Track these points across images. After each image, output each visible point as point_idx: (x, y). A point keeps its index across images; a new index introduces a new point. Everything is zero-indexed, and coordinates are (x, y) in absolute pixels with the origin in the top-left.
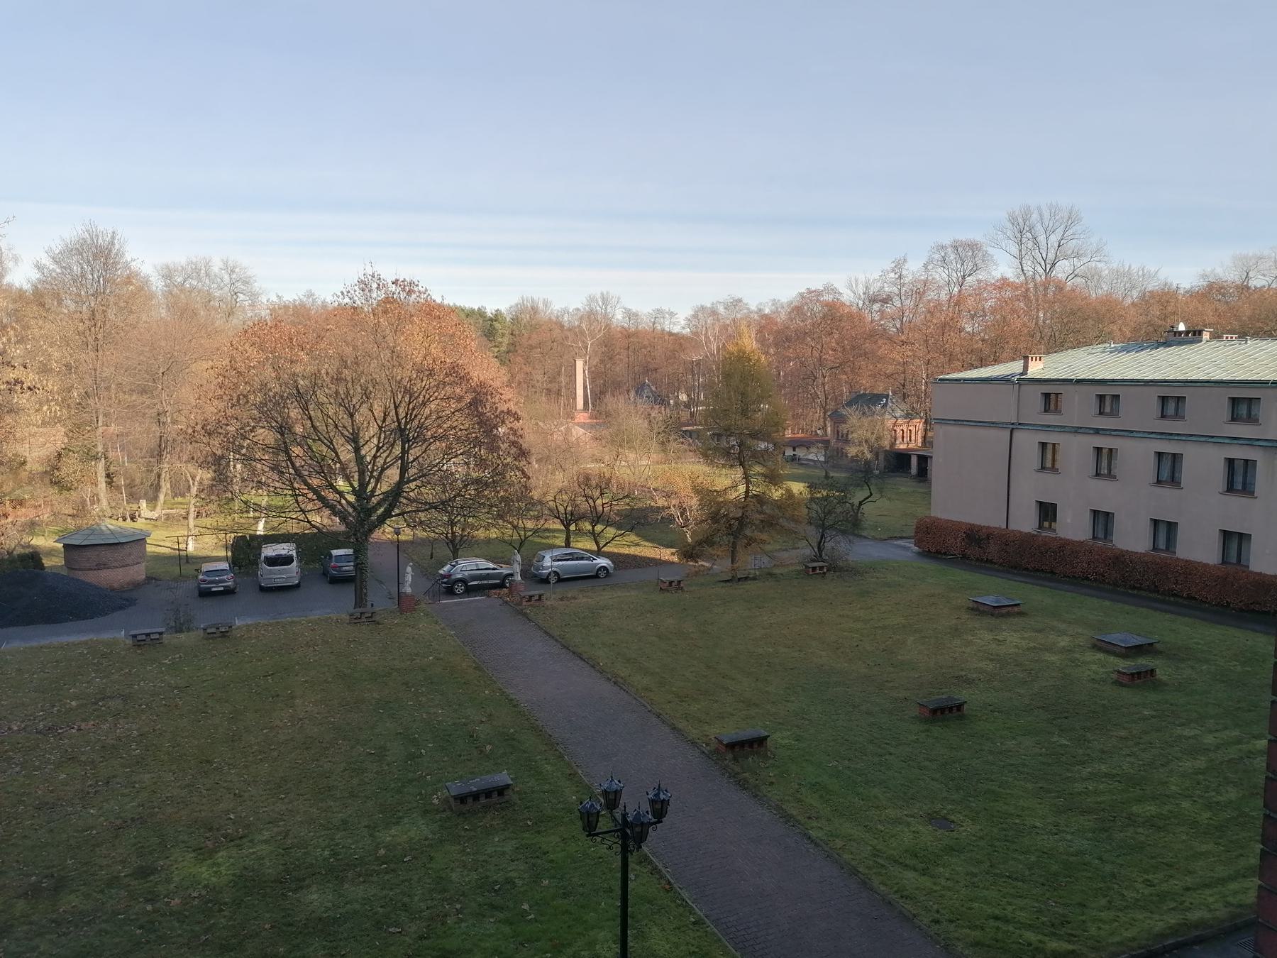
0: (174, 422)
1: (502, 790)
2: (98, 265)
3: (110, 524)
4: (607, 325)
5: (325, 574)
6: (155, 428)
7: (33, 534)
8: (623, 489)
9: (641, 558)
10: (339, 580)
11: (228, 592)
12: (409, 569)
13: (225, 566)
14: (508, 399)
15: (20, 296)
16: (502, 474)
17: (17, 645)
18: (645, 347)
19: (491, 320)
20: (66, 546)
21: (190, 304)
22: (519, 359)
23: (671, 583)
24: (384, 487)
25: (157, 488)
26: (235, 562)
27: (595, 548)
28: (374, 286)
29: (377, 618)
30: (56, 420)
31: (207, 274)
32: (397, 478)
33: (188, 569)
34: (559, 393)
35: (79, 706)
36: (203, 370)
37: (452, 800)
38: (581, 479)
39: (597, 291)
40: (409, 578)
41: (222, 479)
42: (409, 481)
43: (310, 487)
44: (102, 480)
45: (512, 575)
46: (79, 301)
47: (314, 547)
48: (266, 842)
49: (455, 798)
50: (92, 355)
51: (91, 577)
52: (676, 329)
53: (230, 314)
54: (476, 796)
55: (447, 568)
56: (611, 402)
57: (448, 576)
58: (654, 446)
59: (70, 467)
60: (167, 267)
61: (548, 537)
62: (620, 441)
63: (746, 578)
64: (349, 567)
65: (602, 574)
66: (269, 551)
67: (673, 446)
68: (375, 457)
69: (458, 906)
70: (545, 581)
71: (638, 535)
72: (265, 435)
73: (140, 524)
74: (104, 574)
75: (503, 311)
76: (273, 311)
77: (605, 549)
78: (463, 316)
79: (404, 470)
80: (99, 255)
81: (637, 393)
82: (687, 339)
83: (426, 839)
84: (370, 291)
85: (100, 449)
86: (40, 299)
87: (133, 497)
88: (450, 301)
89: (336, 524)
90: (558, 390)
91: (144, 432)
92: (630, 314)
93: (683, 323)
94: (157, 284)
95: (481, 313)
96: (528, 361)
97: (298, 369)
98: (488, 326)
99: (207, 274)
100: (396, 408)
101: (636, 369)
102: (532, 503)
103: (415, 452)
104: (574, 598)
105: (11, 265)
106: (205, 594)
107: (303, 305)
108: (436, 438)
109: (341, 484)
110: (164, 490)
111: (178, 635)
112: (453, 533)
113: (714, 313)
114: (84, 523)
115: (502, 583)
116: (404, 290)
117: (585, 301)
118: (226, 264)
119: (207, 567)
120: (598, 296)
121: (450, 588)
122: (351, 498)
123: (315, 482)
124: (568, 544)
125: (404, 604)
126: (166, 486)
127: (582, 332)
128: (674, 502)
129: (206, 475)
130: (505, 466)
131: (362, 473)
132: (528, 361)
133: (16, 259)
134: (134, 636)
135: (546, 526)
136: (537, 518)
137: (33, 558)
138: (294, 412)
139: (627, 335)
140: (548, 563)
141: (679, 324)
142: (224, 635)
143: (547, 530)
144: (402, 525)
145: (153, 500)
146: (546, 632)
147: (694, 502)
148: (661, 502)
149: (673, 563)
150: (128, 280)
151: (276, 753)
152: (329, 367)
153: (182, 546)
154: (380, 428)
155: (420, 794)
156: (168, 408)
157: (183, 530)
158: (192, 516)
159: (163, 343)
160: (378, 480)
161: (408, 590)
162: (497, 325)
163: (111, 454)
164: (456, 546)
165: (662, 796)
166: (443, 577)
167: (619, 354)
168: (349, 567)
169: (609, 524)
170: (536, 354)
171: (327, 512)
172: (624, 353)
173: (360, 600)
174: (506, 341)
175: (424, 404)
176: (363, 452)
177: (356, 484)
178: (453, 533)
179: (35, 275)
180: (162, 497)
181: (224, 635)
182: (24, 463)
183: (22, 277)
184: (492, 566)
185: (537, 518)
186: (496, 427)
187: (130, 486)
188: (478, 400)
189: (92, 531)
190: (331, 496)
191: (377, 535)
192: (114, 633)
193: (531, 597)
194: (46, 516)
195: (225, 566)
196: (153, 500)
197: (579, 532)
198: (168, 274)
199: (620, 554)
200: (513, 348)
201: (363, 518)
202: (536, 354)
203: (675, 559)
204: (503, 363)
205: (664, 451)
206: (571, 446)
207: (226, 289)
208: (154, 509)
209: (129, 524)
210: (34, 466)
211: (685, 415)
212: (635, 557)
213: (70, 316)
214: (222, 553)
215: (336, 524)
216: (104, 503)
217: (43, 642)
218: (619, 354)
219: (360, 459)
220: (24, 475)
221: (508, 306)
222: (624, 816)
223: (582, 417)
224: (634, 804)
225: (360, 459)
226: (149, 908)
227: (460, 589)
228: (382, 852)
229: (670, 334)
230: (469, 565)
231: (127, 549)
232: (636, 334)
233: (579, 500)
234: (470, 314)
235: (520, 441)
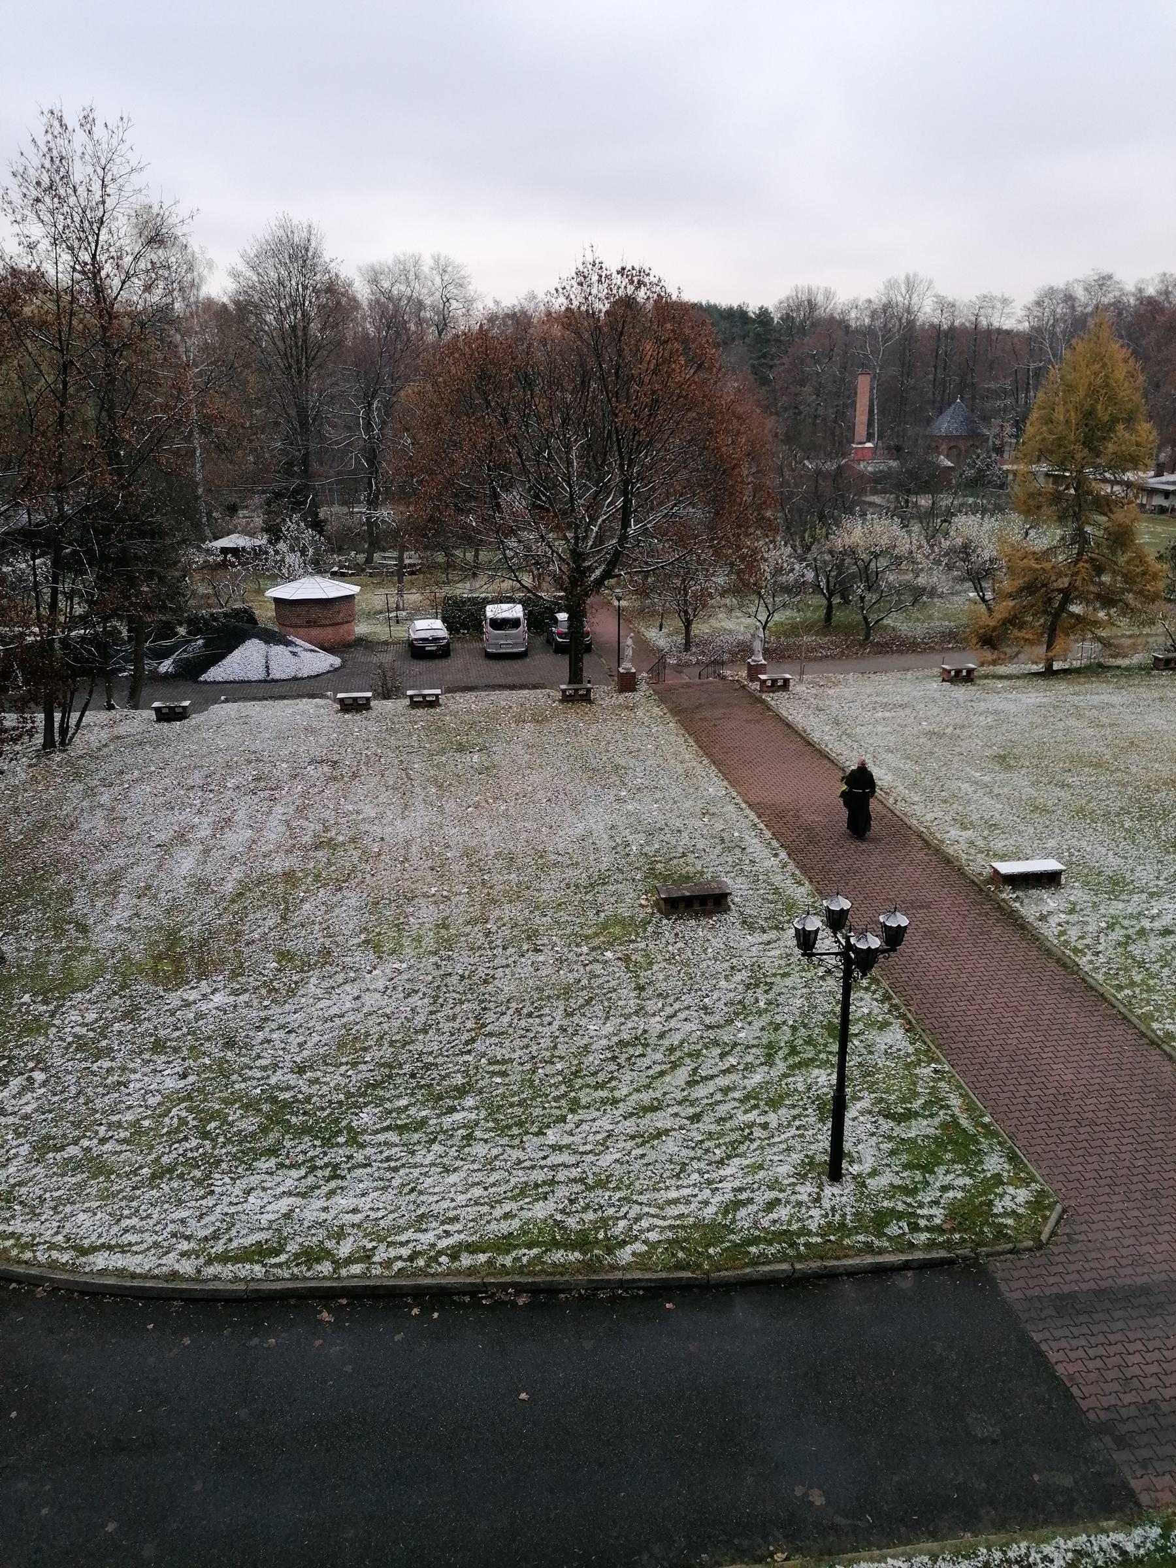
2: (295, 268)
12: (629, 642)
28: (595, 278)
31: (417, 277)
37: (662, 903)
52: (1008, 324)
60: (373, 269)
63: (267, 667)
75: (771, 309)
76: (492, 319)
80: (298, 254)
93: (1020, 313)
94: (362, 291)
99: (417, 277)
105: (205, 272)
107: (524, 313)
111: (385, 702)
113: (1069, 298)
117: (882, 288)
118: (437, 262)
120: (902, 280)
133: (210, 265)
141: (1013, 318)
183: (218, 287)
207: (438, 294)
231: (336, 608)
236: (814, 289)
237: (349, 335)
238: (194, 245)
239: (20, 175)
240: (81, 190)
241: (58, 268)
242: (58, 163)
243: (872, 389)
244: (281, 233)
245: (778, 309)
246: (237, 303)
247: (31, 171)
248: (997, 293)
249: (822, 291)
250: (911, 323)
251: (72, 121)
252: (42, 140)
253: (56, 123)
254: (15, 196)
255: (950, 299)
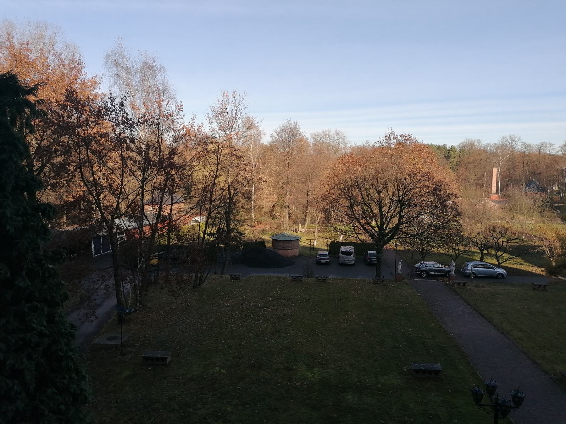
0: (313, 195)
1: (437, 372)
3: (288, 233)
4: (512, 152)
5: (365, 260)
6: (306, 197)
7: (264, 234)
8: (515, 234)
9: (524, 271)
10: (370, 264)
11: (327, 264)
12: (400, 263)
13: (327, 253)
14: (454, 187)
15: (265, 147)
16: (448, 224)
17: (256, 275)
18: (534, 162)
19: (449, 150)
20: (273, 240)
21: (322, 148)
22: (462, 169)
23: (540, 286)
24: (391, 226)
25: (305, 220)
26: (330, 252)
27: (497, 263)
28: (392, 138)
29: (385, 283)
30: (274, 193)
31: (329, 136)
32: (397, 222)
33: (314, 253)
34: (482, 185)
35: (272, 300)
36: (324, 174)
38: (491, 228)
39: (507, 135)
40: (400, 267)
41: (328, 219)
42: (403, 224)
43: (360, 223)
44: (287, 216)
45: (450, 271)
46: (284, 149)
47: (361, 248)
48: (333, 369)
49: (414, 370)
50: (287, 169)
51: (281, 252)
52: (553, 153)
53: (336, 152)
54: (424, 372)
55: (418, 265)
56: (511, 190)
57: (419, 268)
58: (536, 213)
59: (277, 210)
60: (315, 134)
61: (471, 255)
62: (515, 210)
64: (374, 259)
65: (500, 277)
66: (344, 249)
67: (547, 214)
68: (388, 212)
69: (412, 420)
70: (468, 276)
71: (522, 259)
72: (344, 201)
73: (298, 234)
74: (285, 251)
76: (353, 149)
77: (503, 264)
78: (436, 149)
79: (400, 219)
80: (291, 131)
81: (527, 186)
82: (559, 157)
83: (400, 385)
84: (390, 140)
85: (287, 204)
86: (271, 148)
87: (297, 223)
88: (426, 142)
89: (369, 240)
90: (482, 184)
91: (302, 199)
92: (525, 145)
93: (558, 149)
94: (311, 141)
95: (444, 147)
96: (467, 169)
97: (358, 174)
98: (447, 153)
99: (329, 136)
100: (398, 191)
101: (528, 173)
102: (462, 239)
103: (405, 211)
104: (483, 287)
106: (319, 263)
107: (364, 147)
108: (417, 205)
109: (374, 223)
110: (307, 221)
112: (422, 249)
114: (280, 231)
115: (446, 274)
116: (405, 139)
118: (336, 132)
119: (320, 253)
121: (419, 273)
122: (377, 229)
123: (363, 221)
124: (482, 260)
125: (398, 279)
126: (308, 220)
127: (497, 155)
128: (545, 243)
129: (321, 216)
130: (449, 220)
131: (382, 219)
132: (467, 169)
133: (265, 134)
134: (292, 277)
135: (470, 250)
136: (466, 245)
137: (263, 243)
138: (356, 192)
139: (523, 156)
140: (470, 268)
142: (324, 281)
143: (470, 251)
144: (398, 243)
145: (303, 224)
146: (465, 301)
147: (557, 244)
148: (538, 243)
149: (543, 276)
150: (300, 140)
151: (339, 333)
152: (372, 173)
153: (312, 244)
154: (391, 199)
155: (398, 364)
156: (311, 189)
157: (312, 237)
158: (316, 232)
159: (311, 164)
160: (389, 222)
161: (400, 272)
162: (451, 153)
163: (291, 206)
164: (424, 255)
165: (519, 395)
166: (416, 268)
167: (518, 166)
168: (374, 259)
169: (505, 251)
170: (471, 166)
171: (367, 235)
172: (521, 165)
173: (378, 274)
174: (455, 161)
175: (411, 190)
176: (383, 210)
177: (379, 224)
178: (422, 249)
179: (270, 139)
180: (307, 224)
181: (324, 281)
182: (263, 208)
183: (266, 140)
184: (441, 266)
185: (466, 245)
186: (445, 201)
187: (296, 219)
188: (438, 187)
189: (282, 235)
190: (367, 227)
191: (387, 246)
192: (272, 274)
193: (459, 283)
194: (268, 228)
195: (327, 253)
196: (303, 224)
197: (489, 254)
198: (315, 137)
199: (511, 268)
200: (459, 164)
201: (382, 238)
202: (471, 166)
203: (544, 273)
204: (453, 171)
205: (542, 216)
206: (485, 211)
208: (303, 228)
209: (295, 233)
210: (266, 210)
211: (556, 198)
212: (520, 270)
213: (280, 154)
214: (326, 248)
215: (369, 240)
216: (287, 224)
217: (263, 275)
218: (518, 166)
219: (381, 212)
220: (263, 212)
221: (458, 144)
222: (497, 399)
223: (495, 197)
224: (504, 394)
225: (381, 212)
226: (289, 384)
227: (424, 275)
228: (380, 386)
229: (550, 155)
230: (429, 264)
232: (529, 155)
233: (489, 238)
234: (439, 148)
235: (458, 208)
236: (473, 139)
237: (305, 154)
238: (261, 128)
239: (213, 110)
240: (230, 114)
241: (219, 135)
242: (224, 107)
243: (497, 174)
244: (288, 124)
245: (459, 146)
246: (270, 144)
247: (216, 108)
248: (547, 141)
249: (476, 140)
250: (512, 152)
251: (230, 94)
252: (221, 99)
253: (225, 95)
254: (211, 116)
255: (528, 143)
